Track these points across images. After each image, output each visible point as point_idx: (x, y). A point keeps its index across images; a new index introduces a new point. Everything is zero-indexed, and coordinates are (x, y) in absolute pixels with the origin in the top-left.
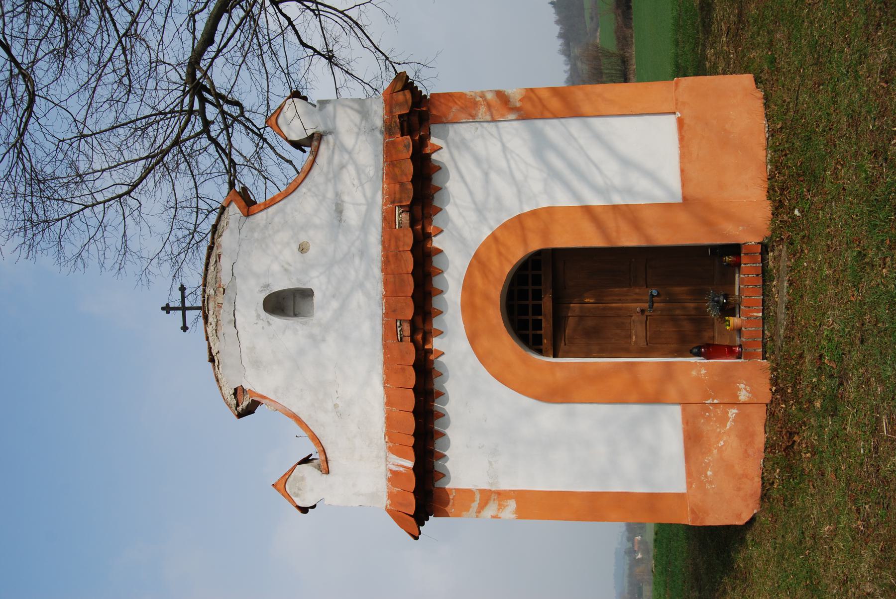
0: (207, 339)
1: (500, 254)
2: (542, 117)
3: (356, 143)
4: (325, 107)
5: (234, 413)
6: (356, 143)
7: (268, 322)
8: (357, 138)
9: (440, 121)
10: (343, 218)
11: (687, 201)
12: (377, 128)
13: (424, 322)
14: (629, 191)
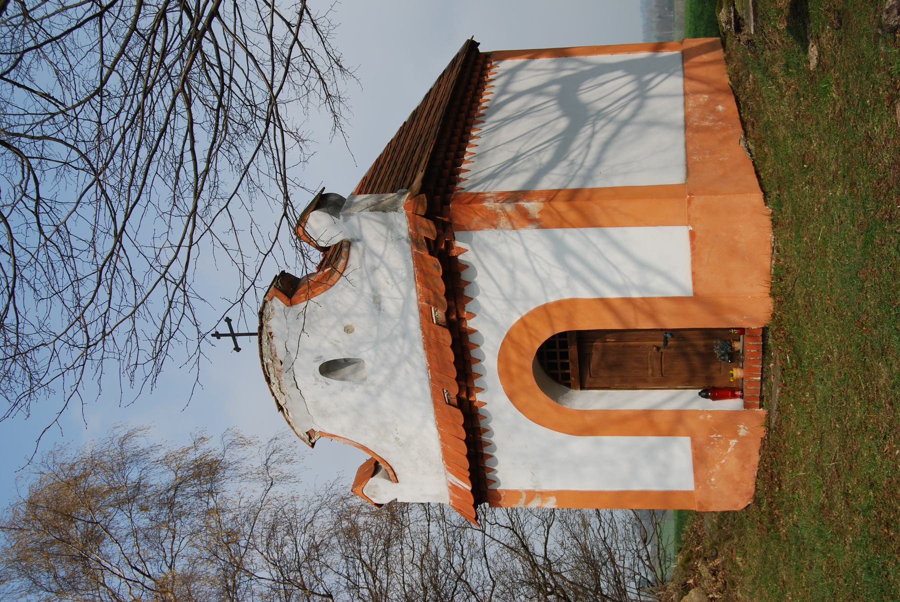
0: (273, 394)
1: (530, 335)
2: (561, 226)
3: (385, 249)
4: (349, 219)
5: (308, 444)
6: (385, 249)
7: (326, 383)
8: (386, 246)
9: (461, 228)
10: (382, 308)
12: (403, 238)
13: (466, 382)
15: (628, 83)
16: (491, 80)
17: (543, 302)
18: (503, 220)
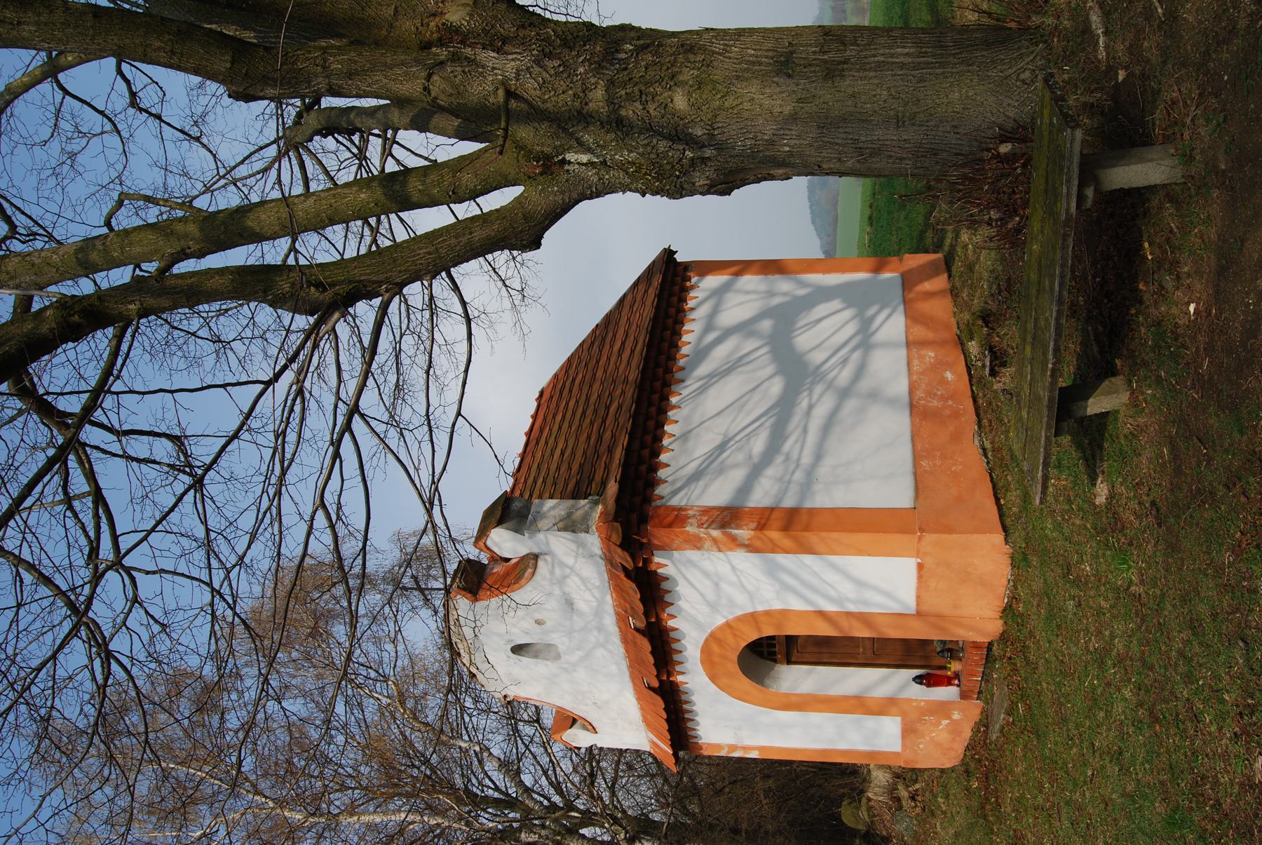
2: (773, 551)
3: (576, 562)
6: (576, 562)
9: (661, 548)
11: (919, 614)
14: (865, 603)
15: (847, 322)
16: (692, 309)
17: (751, 610)
18: (708, 544)
